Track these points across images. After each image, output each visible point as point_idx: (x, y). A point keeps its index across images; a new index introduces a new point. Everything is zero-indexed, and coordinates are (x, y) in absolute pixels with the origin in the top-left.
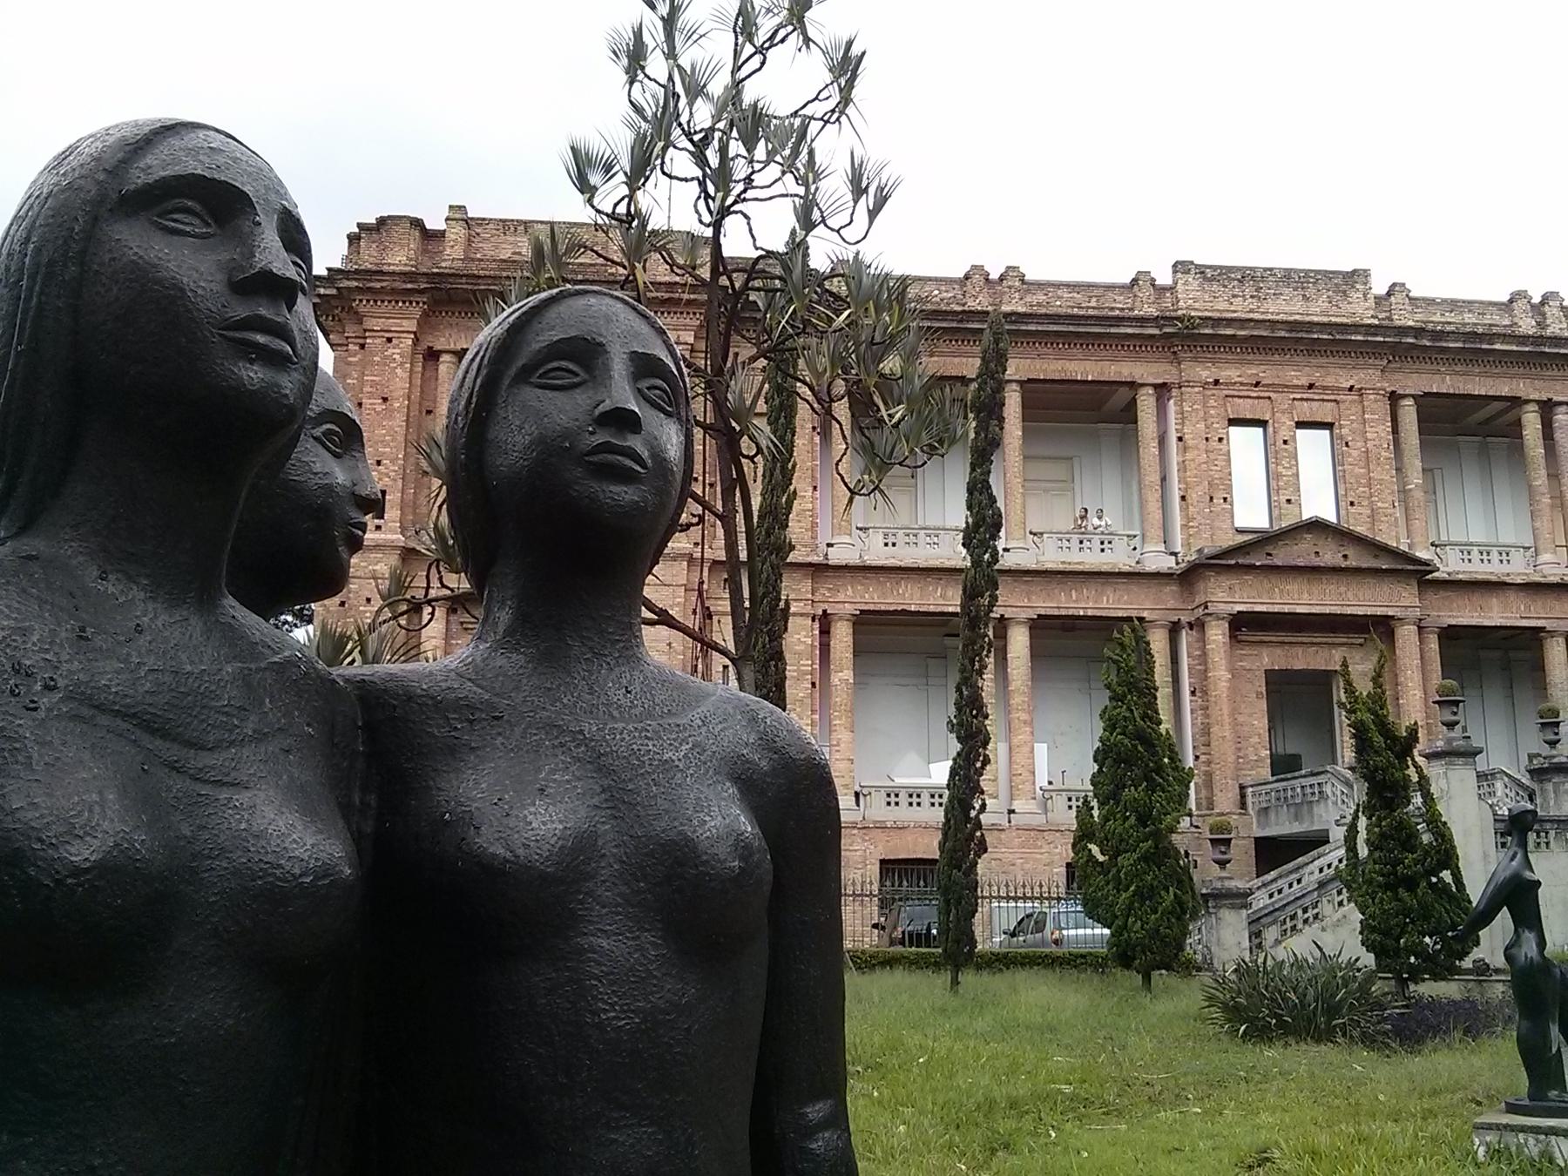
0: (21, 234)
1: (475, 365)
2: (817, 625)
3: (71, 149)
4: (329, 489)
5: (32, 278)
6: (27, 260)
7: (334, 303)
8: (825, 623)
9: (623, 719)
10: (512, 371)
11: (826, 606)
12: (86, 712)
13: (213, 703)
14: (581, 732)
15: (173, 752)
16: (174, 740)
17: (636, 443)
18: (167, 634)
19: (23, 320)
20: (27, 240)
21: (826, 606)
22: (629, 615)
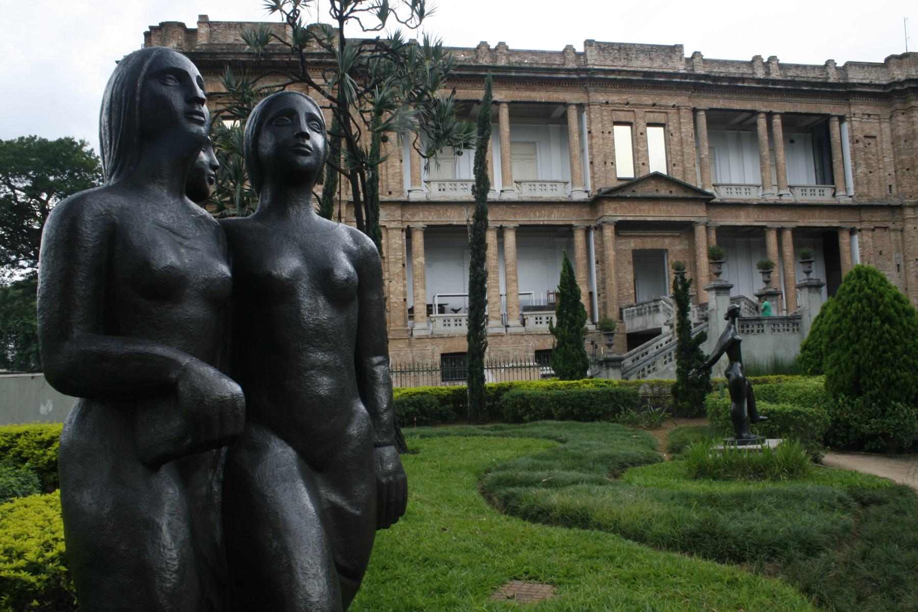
2: (404, 234)
5: (126, 101)
8: (409, 233)
11: (409, 224)
15: (178, 239)
17: (308, 143)
21: (409, 224)
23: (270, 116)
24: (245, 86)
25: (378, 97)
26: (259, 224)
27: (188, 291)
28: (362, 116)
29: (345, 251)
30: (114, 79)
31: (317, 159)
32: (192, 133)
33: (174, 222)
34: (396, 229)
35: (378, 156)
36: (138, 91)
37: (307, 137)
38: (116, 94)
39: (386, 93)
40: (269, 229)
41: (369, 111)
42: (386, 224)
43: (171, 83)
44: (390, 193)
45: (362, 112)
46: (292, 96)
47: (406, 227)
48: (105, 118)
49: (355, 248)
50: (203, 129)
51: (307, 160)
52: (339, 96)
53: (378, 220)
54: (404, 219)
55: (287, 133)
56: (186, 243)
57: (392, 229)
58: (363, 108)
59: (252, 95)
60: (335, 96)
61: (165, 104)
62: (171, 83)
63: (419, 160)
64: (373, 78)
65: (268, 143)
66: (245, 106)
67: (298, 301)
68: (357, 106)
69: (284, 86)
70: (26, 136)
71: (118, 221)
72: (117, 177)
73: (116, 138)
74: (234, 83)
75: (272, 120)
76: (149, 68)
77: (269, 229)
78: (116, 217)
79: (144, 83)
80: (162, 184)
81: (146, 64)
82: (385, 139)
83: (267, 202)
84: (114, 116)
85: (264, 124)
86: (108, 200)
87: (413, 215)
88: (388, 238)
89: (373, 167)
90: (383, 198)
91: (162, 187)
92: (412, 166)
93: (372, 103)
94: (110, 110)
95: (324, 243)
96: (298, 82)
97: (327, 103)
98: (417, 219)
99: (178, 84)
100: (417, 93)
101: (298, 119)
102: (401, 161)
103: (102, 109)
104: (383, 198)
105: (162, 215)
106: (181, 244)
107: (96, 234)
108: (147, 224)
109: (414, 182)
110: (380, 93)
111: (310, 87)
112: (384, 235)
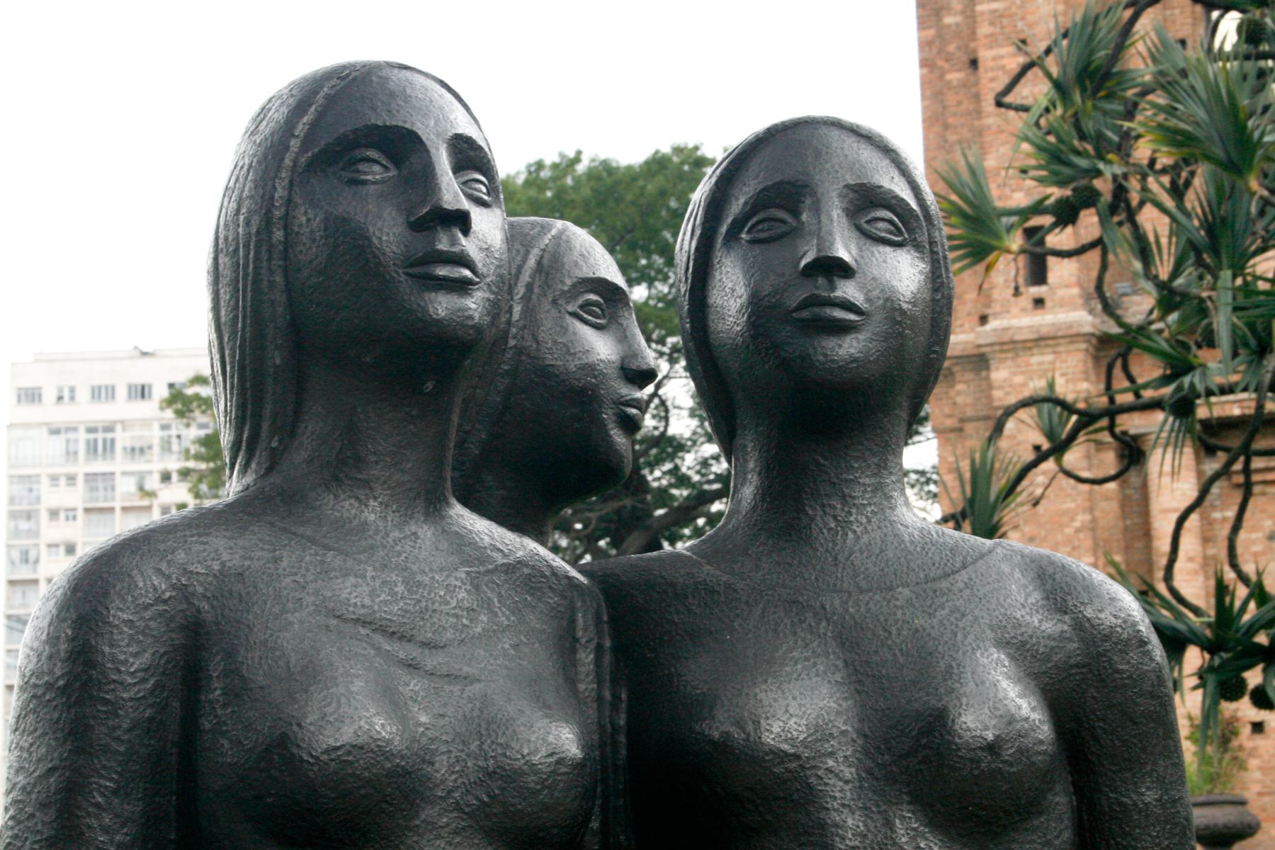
0: (233, 205)
3: (264, 111)
4: (590, 368)
5: (247, 246)
10: (724, 229)
14: (823, 607)
16: (409, 641)
17: (848, 290)
18: (398, 548)
19: (245, 286)
20: (238, 211)
23: (736, 207)
27: (428, 813)
29: (1002, 644)
43: (374, 173)
51: (849, 348)
56: (432, 661)
61: (350, 243)
67: (823, 826)
70: (550, 158)
78: (205, 606)
85: (720, 240)
86: (181, 556)
99: (393, 172)
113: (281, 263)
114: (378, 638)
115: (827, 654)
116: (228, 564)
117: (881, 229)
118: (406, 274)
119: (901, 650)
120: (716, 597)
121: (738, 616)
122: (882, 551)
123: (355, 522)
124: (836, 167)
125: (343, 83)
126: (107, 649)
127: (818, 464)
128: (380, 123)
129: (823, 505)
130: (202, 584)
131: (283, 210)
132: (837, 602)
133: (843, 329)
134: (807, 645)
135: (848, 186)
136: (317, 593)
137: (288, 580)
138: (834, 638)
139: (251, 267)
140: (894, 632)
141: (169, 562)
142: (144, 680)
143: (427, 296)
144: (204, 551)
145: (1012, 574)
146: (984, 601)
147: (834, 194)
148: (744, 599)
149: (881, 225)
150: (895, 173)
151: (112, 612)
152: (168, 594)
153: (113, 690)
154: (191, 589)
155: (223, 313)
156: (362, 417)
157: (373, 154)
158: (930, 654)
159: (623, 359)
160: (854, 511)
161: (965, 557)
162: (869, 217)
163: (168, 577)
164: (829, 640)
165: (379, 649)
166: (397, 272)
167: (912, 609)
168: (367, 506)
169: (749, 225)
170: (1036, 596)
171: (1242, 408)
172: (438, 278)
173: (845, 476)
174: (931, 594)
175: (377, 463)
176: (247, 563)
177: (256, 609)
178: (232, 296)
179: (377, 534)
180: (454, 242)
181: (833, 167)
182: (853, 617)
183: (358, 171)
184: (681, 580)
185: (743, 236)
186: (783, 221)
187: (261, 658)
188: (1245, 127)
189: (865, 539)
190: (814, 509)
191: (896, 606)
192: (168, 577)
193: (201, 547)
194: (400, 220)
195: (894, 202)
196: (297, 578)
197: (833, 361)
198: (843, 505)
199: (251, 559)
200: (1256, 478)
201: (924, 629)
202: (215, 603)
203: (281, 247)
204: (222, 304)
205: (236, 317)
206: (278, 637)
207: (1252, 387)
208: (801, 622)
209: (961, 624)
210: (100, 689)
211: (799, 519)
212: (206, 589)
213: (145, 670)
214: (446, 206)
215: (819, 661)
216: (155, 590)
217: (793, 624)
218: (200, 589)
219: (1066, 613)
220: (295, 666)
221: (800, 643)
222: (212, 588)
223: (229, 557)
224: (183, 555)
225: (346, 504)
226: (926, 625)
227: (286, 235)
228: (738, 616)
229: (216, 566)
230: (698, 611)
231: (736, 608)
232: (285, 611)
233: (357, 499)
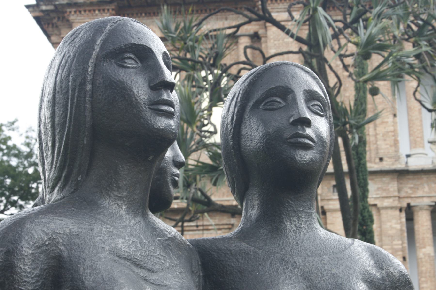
1: (234, 102)
2: (403, 215)
5: (73, 91)
6: (70, 83)
7: (52, 15)
8: (409, 213)
9: (312, 256)
10: (251, 104)
11: (409, 201)
12: (117, 258)
13: (154, 254)
14: (295, 263)
15: (143, 273)
16: (144, 269)
17: (309, 131)
18: (135, 228)
20: (68, 75)
21: (409, 201)
22: (310, 209)
23: (257, 96)
24: (187, 29)
25: (363, 35)
26: (244, 245)
28: (342, 61)
30: (57, 62)
31: (322, 152)
32: (159, 130)
33: (137, 250)
34: (392, 208)
35: (364, 112)
36: (89, 77)
37: (307, 123)
38: (61, 81)
39: (373, 30)
40: (260, 252)
41: (352, 55)
42: (377, 202)
43: (130, 64)
44: (381, 159)
45: (342, 57)
46: (285, 68)
47: (405, 205)
48: (46, 113)
49: (378, 275)
50: (172, 123)
52: (309, 35)
53: (367, 197)
54: (403, 194)
55: (279, 120)
56: (153, 277)
57: (386, 208)
58: (343, 52)
59: (197, 41)
60: (304, 34)
61: (122, 92)
62: (130, 64)
63: (420, 113)
64: (355, 9)
65: (253, 134)
66: (189, 56)
68: (336, 47)
69: (238, 27)
71: (65, 254)
72: (61, 190)
73: (61, 139)
74: (173, 27)
75: (258, 103)
76: (102, 47)
77: (260, 252)
78: (62, 248)
79: (96, 66)
80: (121, 198)
81: (99, 42)
82: (375, 92)
83: (254, 213)
84: (59, 112)
85: (248, 108)
87: (415, 189)
88: (380, 222)
89: (359, 127)
90: (372, 166)
91: (120, 202)
92: (410, 123)
93: (356, 44)
94: (53, 102)
95: (334, 271)
96: (256, 20)
97: (295, 46)
98: (420, 193)
99: (139, 65)
100: (417, 25)
101: (295, 100)
102: (395, 115)
103: (42, 101)
104: (372, 166)
105: (121, 241)
106: (145, 280)
107: (37, 271)
108: (103, 255)
109: (414, 143)
110: (366, 28)
111: (268, 24)
112: (375, 217)
113: (90, 99)
114: (134, 268)
115: (299, 282)
116: (72, 230)
117: (315, 108)
118: (149, 108)
119: (329, 282)
120: (249, 256)
121: (260, 265)
122: (314, 241)
123: (118, 215)
124: (301, 82)
125: (115, 25)
126: (22, 267)
127: (288, 202)
128: (136, 43)
129: (291, 220)
130: (61, 239)
131: (92, 76)
132: (300, 261)
133: (307, 147)
134: (291, 278)
135: (305, 90)
136: (109, 245)
137: (98, 239)
138: (301, 276)
139: (75, 100)
140: (325, 275)
141: (47, 227)
142: (37, 281)
143: (158, 118)
144: (62, 223)
145: (362, 252)
146: (356, 263)
147: (301, 93)
148: (262, 257)
149: (316, 107)
150: (319, 88)
151: (24, 249)
152: (47, 243)
153: (25, 285)
154: (57, 240)
155: (57, 119)
156: (121, 169)
157: (132, 56)
158: (341, 284)
159: (174, 157)
160: (303, 223)
161: (345, 245)
162: (313, 104)
163: (47, 234)
164: (299, 277)
165: (134, 272)
166: (145, 107)
167: (330, 265)
168: (122, 208)
169: (264, 103)
170: (372, 262)
171: (178, 205)
172: (162, 111)
173: (299, 209)
174: (337, 259)
175: (126, 190)
176: (80, 230)
177: (86, 251)
178: (63, 112)
179: (127, 221)
180: (169, 97)
181: (299, 82)
182: (307, 268)
183: (126, 63)
184: (234, 248)
185: (261, 107)
186: (280, 103)
187: (90, 273)
188: (193, 109)
189: (307, 235)
190: (287, 221)
191: (324, 264)
192: (47, 234)
193: (61, 222)
194: (146, 85)
195: (321, 98)
196: (101, 238)
197: (304, 161)
198: (298, 221)
199: (82, 228)
200: (185, 228)
201: (337, 274)
202: (68, 247)
203: (90, 92)
204: (57, 115)
205: (65, 121)
206: (97, 264)
207: (185, 198)
208: (287, 268)
209: (350, 272)
210: (19, 285)
211: (281, 225)
212: (63, 241)
213: (38, 276)
214: (168, 80)
215: (297, 285)
216: (42, 240)
217: (284, 269)
218: (61, 241)
219: (383, 270)
220: (105, 278)
221: (288, 277)
222: (66, 241)
223: (72, 227)
224: (53, 225)
225: (114, 207)
226: (337, 272)
227: (93, 87)
228: (260, 265)
229: (67, 231)
230: (242, 262)
231: (259, 261)
232: (98, 253)
233: (118, 205)
